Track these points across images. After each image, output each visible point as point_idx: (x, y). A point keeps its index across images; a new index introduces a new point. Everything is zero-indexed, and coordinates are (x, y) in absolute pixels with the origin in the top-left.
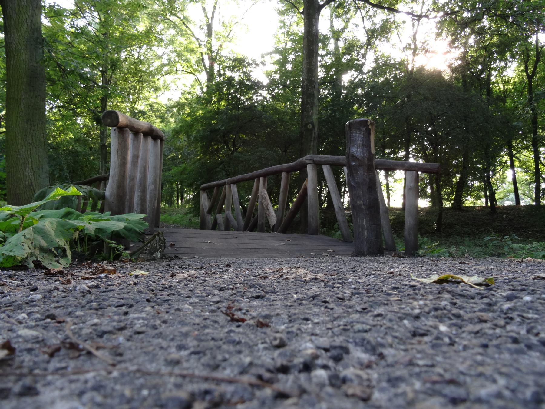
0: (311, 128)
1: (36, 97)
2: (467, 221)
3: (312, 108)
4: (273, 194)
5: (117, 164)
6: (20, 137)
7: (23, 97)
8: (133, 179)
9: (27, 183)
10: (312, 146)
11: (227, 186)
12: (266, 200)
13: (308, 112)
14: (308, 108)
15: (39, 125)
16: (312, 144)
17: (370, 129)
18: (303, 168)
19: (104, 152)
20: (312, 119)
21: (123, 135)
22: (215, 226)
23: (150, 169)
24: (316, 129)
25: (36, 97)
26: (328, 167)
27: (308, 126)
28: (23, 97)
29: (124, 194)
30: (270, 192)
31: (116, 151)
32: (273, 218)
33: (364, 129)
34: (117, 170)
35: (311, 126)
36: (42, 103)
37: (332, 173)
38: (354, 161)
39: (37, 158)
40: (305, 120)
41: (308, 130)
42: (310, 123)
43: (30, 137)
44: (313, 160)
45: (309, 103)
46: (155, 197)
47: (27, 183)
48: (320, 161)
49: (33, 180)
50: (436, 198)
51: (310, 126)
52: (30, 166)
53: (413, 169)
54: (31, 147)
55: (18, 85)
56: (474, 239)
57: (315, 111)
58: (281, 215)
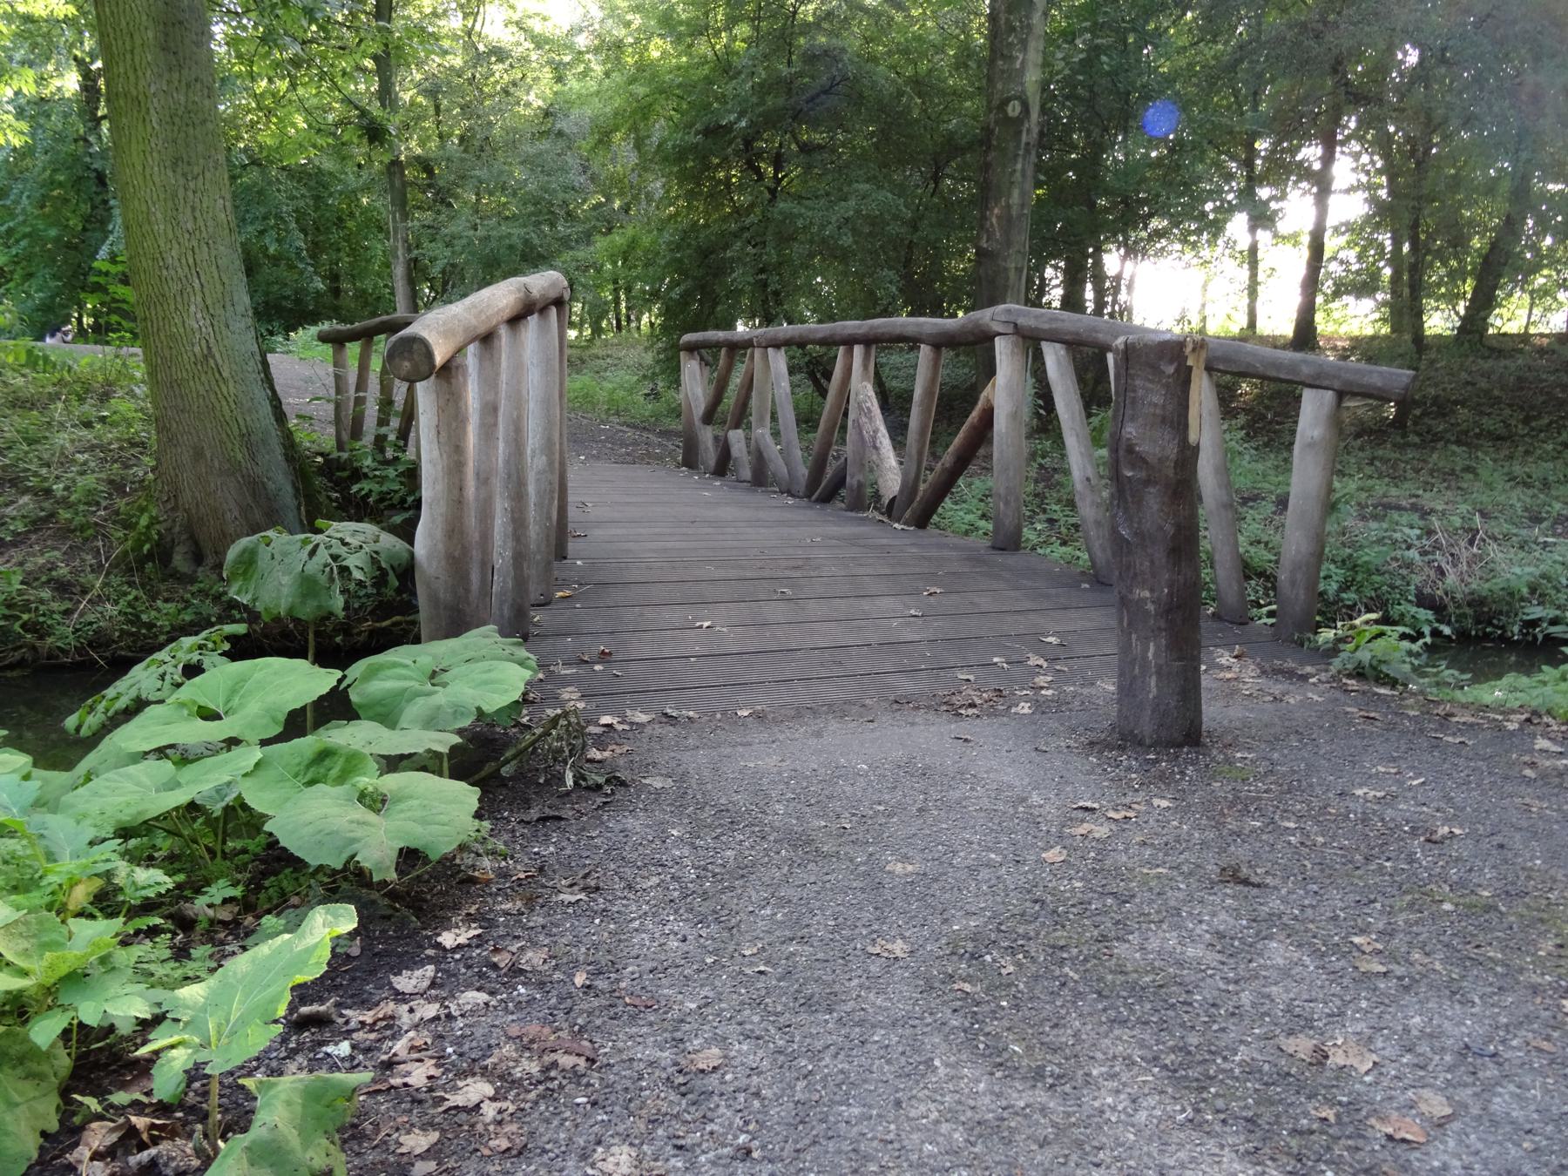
0: (1016, 113)
1: (188, 86)
2: (1496, 393)
3: (1024, 44)
5: (439, 467)
6: (159, 215)
7: (153, 89)
8: (487, 567)
9: (197, 349)
10: (1018, 174)
11: (758, 353)
12: (870, 419)
13: (1011, 59)
14: (1011, 44)
15: (208, 175)
16: (1019, 166)
17: (1190, 368)
18: (978, 345)
19: (397, 183)
20: (1022, 84)
21: (449, 383)
22: (723, 466)
23: (532, 405)
25: (188, 86)
26: (1060, 349)
27: (1009, 109)
28: (153, 89)
29: (465, 550)
31: (434, 432)
32: (890, 476)
33: (1170, 369)
34: (439, 487)
35: (1018, 109)
36: (207, 102)
37: (1071, 369)
38: (1133, 467)
40: (999, 86)
42: (1016, 98)
43: (188, 210)
44: (1016, 325)
45: (1013, 29)
46: (552, 491)
47: (197, 349)
48: (1037, 329)
49: (212, 341)
50: (1406, 311)
51: (1014, 109)
52: (199, 299)
53: (1326, 383)
55: (132, 52)
56: (1511, 457)
57: (1034, 55)
58: (912, 475)
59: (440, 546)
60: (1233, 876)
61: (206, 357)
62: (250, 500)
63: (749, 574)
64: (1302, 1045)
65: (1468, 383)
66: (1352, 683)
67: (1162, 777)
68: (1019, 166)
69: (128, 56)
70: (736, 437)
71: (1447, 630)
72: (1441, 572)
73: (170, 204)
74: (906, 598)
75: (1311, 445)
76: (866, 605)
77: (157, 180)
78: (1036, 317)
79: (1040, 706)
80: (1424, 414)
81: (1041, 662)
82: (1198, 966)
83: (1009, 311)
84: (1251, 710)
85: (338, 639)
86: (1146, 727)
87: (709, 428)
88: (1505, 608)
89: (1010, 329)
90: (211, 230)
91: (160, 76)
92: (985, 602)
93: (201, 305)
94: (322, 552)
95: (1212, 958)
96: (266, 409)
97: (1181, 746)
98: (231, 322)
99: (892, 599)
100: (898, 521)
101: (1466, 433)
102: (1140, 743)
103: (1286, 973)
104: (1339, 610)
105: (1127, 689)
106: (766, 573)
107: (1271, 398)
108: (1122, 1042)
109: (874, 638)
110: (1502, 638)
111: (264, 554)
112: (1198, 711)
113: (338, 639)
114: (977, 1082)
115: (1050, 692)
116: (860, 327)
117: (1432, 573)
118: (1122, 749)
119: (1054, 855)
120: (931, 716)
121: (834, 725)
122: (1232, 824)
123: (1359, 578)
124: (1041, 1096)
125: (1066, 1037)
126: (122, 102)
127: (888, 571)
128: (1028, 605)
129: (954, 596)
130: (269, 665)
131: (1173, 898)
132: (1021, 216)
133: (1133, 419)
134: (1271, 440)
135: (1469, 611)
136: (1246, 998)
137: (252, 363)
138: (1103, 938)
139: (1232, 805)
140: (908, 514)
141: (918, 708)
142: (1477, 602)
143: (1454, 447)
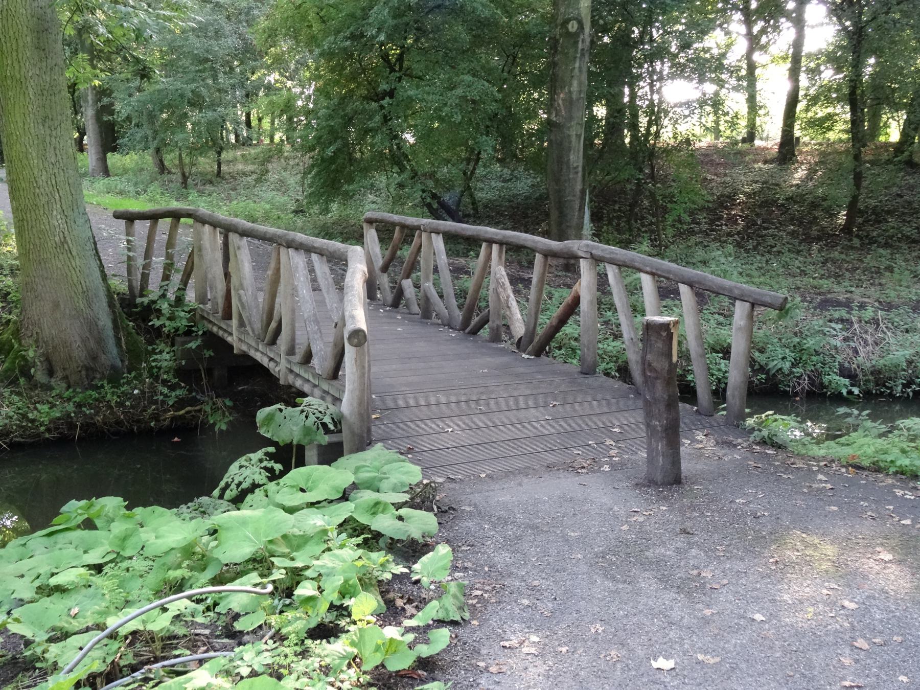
0: (574, 30)
1: (51, 69)
4: (519, 282)
6: (34, 154)
9: (57, 239)
10: (576, 71)
12: (504, 289)
15: (63, 125)
16: (577, 65)
20: (578, 9)
24: (587, 29)
27: (570, 26)
30: (514, 280)
31: (354, 361)
33: (664, 334)
35: (576, 26)
38: (651, 371)
39: (68, 189)
40: (562, 10)
41: (569, 34)
47: (57, 239)
49: (66, 232)
51: (573, 27)
52: (59, 206)
54: (56, 171)
59: (356, 410)
60: (685, 531)
61: (62, 244)
62: (88, 334)
63: (460, 399)
64: (695, 572)
65: (898, 195)
66: (757, 448)
67: (665, 498)
68: (577, 65)
69: (14, 54)
70: (407, 284)
71: (856, 391)
72: (856, 352)
73: (41, 147)
74: (542, 409)
75: (739, 329)
76: (522, 414)
77: (32, 131)
78: (602, 250)
79: (613, 466)
80: (867, 221)
81: (612, 443)
82: (670, 557)
83: (587, 246)
84: (706, 465)
85: (152, 424)
86: (659, 477)
87: (386, 275)
88: (893, 375)
89: (589, 256)
90: (65, 161)
91: (35, 65)
92: (581, 409)
93: (60, 210)
94: (311, 416)
95: (674, 554)
96: (97, 274)
97: (672, 484)
98: (77, 219)
99: (534, 410)
100: (524, 352)
101: (892, 237)
102: (656, 484)
103: (695, 557)
104: (791, 379)
105: (651, 460)
106: (469, 398)
107: (760, 206)
108: (647, 574)
109: (531, 433)
110: (891, 395)
111: (279, 417)
112: (679, 469)
113: (152, 424)
114: (609, 584)
115: (617, 459)
116: (497, 234)
117: (851, 352)
118: (649, 486)
119: (625, 527)
120: (566, 473)
121: (525, 480)
122: (688, 515)
123: (804, 358)
124: (626, 585)
125: (632, 574)
126: (9, 82)
127: (529, 392)
128: (603, 410)
129: (565, 406)
130: (317, 470)
131: (664, 539)
132: (578, 100)
133: (650, 352)
134: (759, 244)
135: (871, 378)
136: (682, 563)
137: (88, 244)
138: (642, 551)
139: (690, 507)
140: (530, 348)
141: (559, 470)
142: (876, 372)
143: (881, 251)
